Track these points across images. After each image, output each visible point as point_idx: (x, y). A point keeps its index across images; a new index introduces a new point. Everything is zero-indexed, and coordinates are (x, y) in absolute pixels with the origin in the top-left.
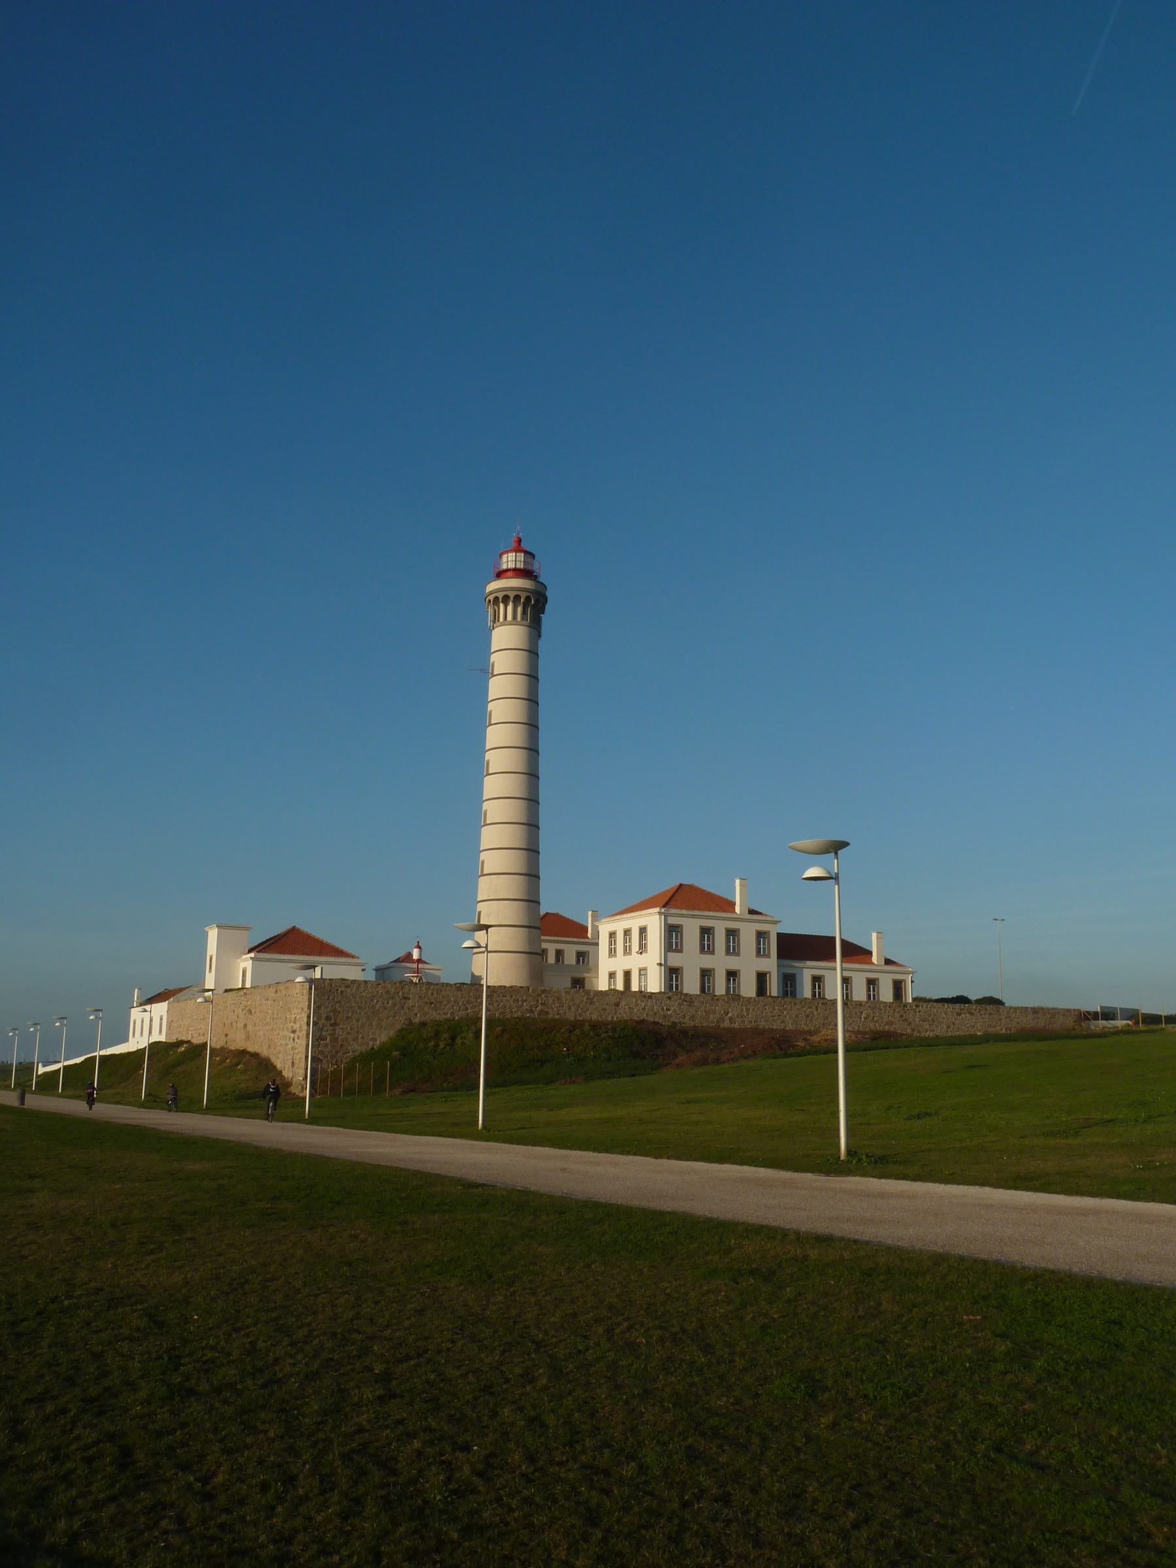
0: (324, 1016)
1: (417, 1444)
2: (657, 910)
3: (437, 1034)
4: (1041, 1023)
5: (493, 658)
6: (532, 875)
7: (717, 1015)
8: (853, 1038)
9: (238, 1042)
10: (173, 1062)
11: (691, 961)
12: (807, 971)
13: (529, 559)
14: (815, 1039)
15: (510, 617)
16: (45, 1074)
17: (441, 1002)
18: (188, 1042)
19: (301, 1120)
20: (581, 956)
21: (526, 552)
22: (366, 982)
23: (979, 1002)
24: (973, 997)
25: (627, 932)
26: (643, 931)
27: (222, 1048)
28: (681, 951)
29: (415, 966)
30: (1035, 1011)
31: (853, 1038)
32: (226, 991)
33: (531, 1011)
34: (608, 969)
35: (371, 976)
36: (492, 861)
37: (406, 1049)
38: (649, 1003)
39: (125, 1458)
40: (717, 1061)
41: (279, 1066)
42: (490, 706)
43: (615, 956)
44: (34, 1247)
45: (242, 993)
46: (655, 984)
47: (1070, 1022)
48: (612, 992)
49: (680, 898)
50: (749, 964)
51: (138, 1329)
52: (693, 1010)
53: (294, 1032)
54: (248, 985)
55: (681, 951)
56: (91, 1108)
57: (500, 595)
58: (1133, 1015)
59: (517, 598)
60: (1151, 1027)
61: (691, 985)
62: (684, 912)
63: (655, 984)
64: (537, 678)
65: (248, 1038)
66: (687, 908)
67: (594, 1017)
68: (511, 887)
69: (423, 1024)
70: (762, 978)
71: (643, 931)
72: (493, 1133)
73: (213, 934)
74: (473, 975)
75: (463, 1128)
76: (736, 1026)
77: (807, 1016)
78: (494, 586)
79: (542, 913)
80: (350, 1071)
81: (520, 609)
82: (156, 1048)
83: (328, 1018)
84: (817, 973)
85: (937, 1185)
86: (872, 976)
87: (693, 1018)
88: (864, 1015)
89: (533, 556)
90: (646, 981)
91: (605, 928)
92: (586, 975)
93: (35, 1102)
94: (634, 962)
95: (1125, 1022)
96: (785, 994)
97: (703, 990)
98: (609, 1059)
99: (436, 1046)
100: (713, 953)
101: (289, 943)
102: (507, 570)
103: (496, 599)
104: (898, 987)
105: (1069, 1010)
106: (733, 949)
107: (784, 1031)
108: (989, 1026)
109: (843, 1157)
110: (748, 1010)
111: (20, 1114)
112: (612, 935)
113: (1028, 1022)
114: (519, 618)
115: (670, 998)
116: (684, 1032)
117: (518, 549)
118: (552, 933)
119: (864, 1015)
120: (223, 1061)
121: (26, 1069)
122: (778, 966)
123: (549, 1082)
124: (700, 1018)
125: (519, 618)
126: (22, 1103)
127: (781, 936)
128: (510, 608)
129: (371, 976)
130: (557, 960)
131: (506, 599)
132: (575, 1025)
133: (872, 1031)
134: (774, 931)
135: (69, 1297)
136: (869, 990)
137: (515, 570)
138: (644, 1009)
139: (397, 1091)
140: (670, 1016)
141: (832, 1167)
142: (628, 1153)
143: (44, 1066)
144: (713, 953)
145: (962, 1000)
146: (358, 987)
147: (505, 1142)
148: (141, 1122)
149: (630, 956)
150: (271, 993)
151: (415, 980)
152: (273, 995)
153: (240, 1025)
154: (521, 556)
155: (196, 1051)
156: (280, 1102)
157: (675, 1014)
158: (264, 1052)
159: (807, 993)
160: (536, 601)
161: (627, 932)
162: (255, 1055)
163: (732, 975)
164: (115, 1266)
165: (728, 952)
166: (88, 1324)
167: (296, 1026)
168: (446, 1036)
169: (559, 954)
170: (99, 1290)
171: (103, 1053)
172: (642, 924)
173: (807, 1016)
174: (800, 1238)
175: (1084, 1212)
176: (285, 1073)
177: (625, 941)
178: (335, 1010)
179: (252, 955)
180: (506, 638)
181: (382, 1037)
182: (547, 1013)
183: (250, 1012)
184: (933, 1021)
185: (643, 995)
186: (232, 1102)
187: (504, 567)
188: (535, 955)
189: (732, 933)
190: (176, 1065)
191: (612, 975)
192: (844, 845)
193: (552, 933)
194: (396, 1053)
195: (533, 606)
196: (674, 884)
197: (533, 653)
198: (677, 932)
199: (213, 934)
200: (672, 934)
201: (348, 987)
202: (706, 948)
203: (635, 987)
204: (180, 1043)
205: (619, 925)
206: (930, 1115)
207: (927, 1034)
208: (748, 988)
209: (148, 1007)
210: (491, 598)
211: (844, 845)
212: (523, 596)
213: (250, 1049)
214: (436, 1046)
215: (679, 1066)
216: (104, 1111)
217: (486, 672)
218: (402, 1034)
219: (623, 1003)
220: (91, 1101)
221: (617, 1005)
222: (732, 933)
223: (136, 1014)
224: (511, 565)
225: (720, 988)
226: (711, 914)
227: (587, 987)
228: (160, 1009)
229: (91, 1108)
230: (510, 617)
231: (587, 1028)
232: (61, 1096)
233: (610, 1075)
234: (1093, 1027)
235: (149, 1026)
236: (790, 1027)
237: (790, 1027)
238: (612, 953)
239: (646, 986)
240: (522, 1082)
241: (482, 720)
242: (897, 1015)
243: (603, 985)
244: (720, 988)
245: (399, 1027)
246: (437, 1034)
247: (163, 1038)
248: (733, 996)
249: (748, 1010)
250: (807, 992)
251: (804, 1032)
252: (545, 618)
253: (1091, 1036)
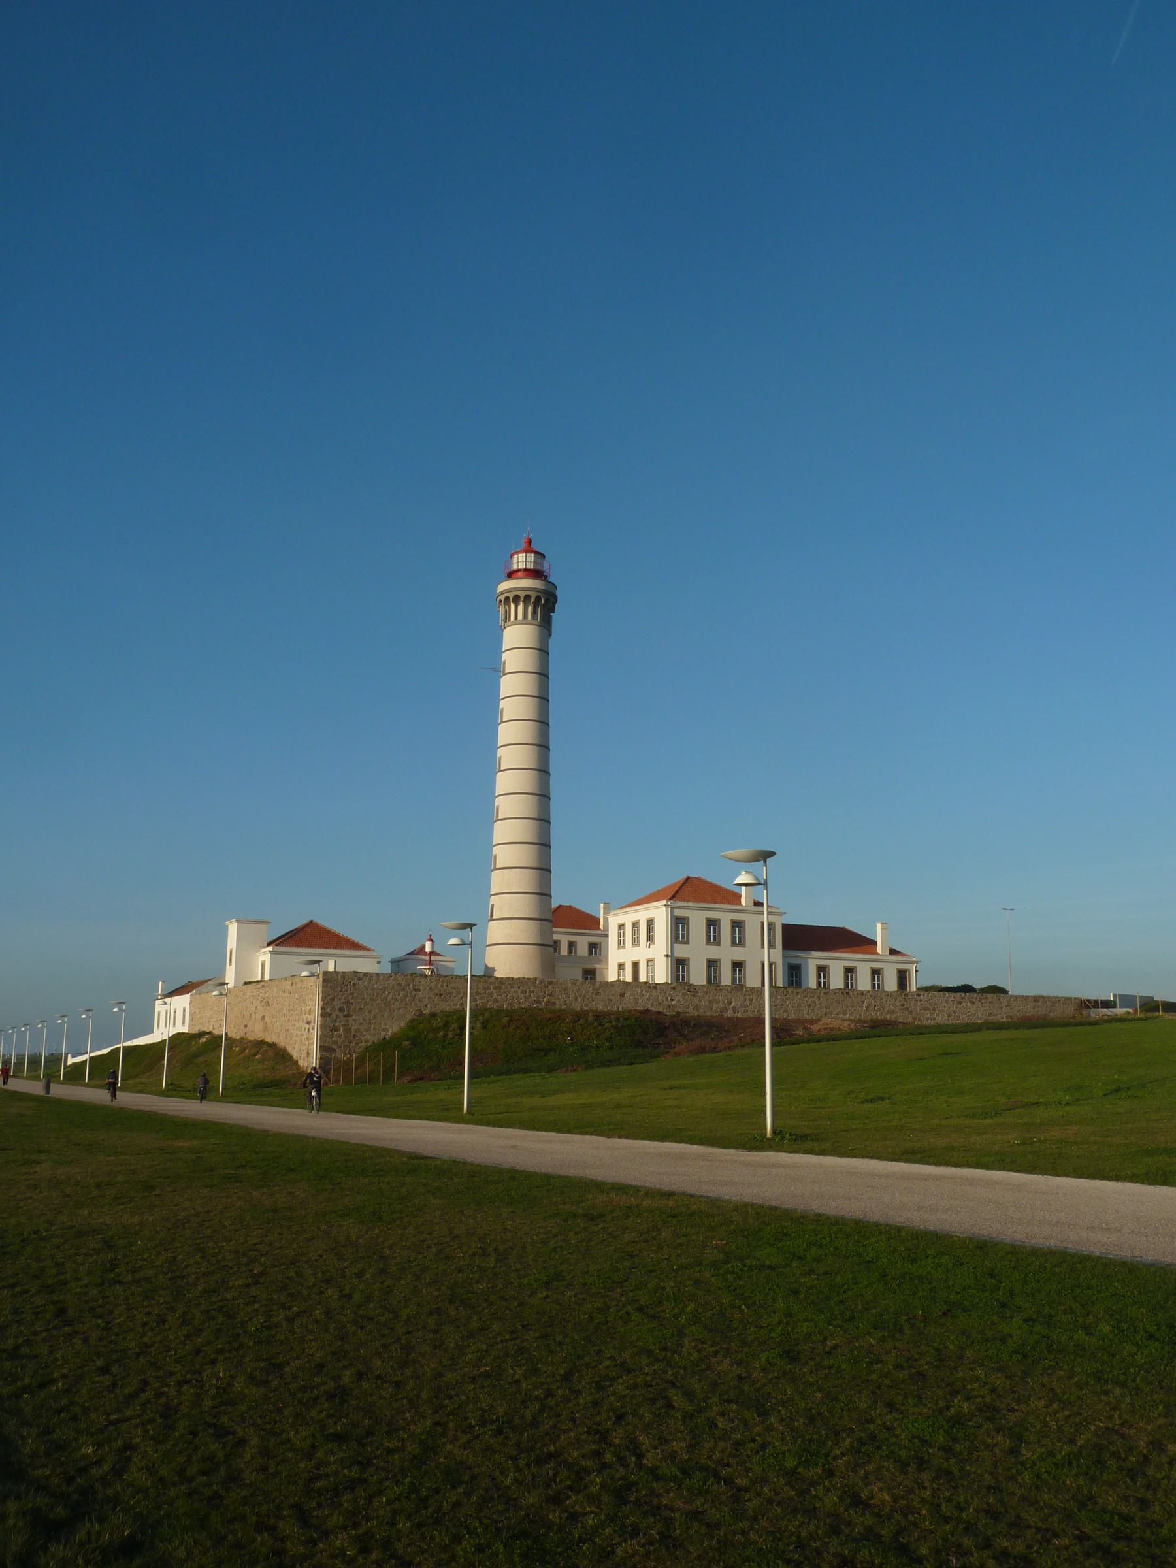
0: (337, 1007)
1: (256, 1306)
2: (664, 902)
3: (447, 1025)
4: (1042, 1010)
5: (505, 656)
6: (543, 869)
7: (721, 1005)
8: (852, 1026)
9: (256, 1033)
10: (194, 1051)
11: (697, 952)
12: (812, 961)
13: (539, 559)
14: (815, 1027)
15: (520, 617)
16: (74, 1064)
17: (450, 994)
18: (210, 1033)
20: (593, 947)
21: (536, 553)
22: (377, 974)
23: (983, 990)
24: (977, 986)
25: (635, 924)
26: (650, 922)
27: (242, 1039)
28: (687, 942)
29: (427, 958)
30: (1036, 999)
31: (852, 1026)
32: (246, 983)
33: (539, 1002)
34: (618, 962)
35: (387, 969)
36: (504, 855)
37: (414, 1039)
38: (654, 993)
39: (62, 1311)
40: (714, 1050)
41: (295, 1055)
42: (502, 704)
43: (638, 945)
44: (30, 1201)
45: (260, 985)
46: (662, 975)
47: (1070, 1011)
48: (620, 982)
49: (689, 890)
51: (94, 1249)
52: (696, 1000)
53: (309, 1023)
54: (267, 978)
55: (687, 942)
57: (511, 595)
58: (1126, 1000)
59: (527, 597)
60: (1150, 1014)
61: (697, 976)
62: (690, 904)
63: (662, 975)
64: (547, 676)
65: (266, 1029)
66: (694, 900)
67: (600, 1007)
68: (522, 880)
69: (434, 1015)
71: (650, 922)
72: (478, 1116)
73: (233, 928)
74: (486, 966)
75: (448, 1112)
76: (739, 1015)
77: (809, 1006)
79: (554, 905)
80: (361, 1060)
81: (530, 609)
82: (178, 1041)
83: (341, 1010)
84: (822, 963)
85: (861, 1160)
86: (876, 965)
87: (696, 1008)
88: (865, 1004)
89: (543, 556)
90: (653, 972)
91: (613, 921)
92: (597, 966)
93: (59, 1091)
94: (641, 953)
95: (1124, 1010)
96: (791, 984)
97: (709, 980)
98: (611, 1048)
99: (445, 1036)
100: (719, 944)
101: (306, 936)
102: (518, 571)
103: (507, 599)
104: (902, 976)
105: (1070, 999)
106: (738, 941)
107: (786, 1020)
108: (990, 1014)
109: (769, 1136)
110: (751, 1000)
111: (44, 1102)
112: (621, 927)
113: (1029, 1010)
114: (529, 617)
115: (674, 988)
116: (686, 1022)
117: (528, 550)
118: (564, 925)
119: (865, 1004)
120: (242, 1051)
121: (54, 1060)
123: (551, 1070)
124: (704, 1008)
125: (529, 617)
126: (48, 1092)
127: (786, 927)
128: (520, 607)
129: (387, 969)
130: (570, 951)
131: (516, 599)
132: (579, 1016)
133: (871, 1020)
134: (779, 922)
135: (47, 1231)
136: (873, 979)
137: (525, 570)
138: (648, 999)
139: (406, 1080)
140: (675, 1006)
141: (757, 1143)
142: (586, 1133)
143: (73, 1057)
144: (719, 944)
145: (967, 989)
146: (370, 980)
147: (482, 1125)
148: (155, 1109)
149: (638, 949)
150: (287, 985)
151: (427, 972)
152: (289, 987)
153: (259, 1016)
154: (531, 557)
155: (215, 1041)
156: (324, 1089)
157: (680, 1004)
158: (281, 1042)
159: (813, 984)
161: (635, 924)
162: (273, 1046)
163: (738, 965)
164: (90, 1214)
165: (734, 943)
166: (58, 1247)
167: (311, 1018)
168: (454, 1026)
169: (572, 945)
170: (72, 1227)
171: (126, 1044)
172: (650, 916)
173: (809, 1006)
174: (649, 1193)
175: (926, 1178)
176: (301, 1063)
177: (634, 933)
178: (347, 1002)
179: (270, 948)
180: (517, 637)
181: (393, 1027)
182: (554, 1004)
183: (268, 1003)
184: (934, 1009)
186: (240, 1092)
187: (515, 567)
188: (547, 948)
189: (737, 925)
190: (197, 1056)
191: (621, 966)
192: (772, 854)
193: (564, 925)
194: (406, 1043)
195: (544, 606)
196: (681, 877)
197: (543, 651)
198: (683, 925)
199: (233, 928)
200: (679, 926)
201: (360, 979)
202: (712, 938)
203: (643, 979)
204: (202, 1034)
205: (627, 917)
206: (882, 1099)
207: (927, 1023)
209: (167, 1000)
210: (502, 597)
211: (772, 854)
212: (533, 595)
213: (268, 1040)
214: (445, 1036)
215: (677, 1054)
216: (126, 1099)
217: (497, 670)
218: (413, 1024)
219: (628, 994)
220: (112, 1088)
221: (622, 995)
222: (737, 925)
223: (159, 1007)
224: (522, 566)
225: (726, 978)
226: (717, 906)
227: (598, 978)
228: (182, 1002)
230: (520, 617)
231: (590, 1019)
232: (86, 1085)
233: (610, 1063)
234: (1093, 1015)
235: (172, 1018)
236: (792, 1016)
237: (793, 1016)
238: (621, 944)
239: (653, 977)
240: (527, 1070)
241: (494, 718)
242: (898, 1004)
243: (612, 976)
244: (726, 978)
245: (409, 1017)
246: (447, 1025)
247: (186, 1030)
248: (738, 986)
249: (751, 1000)
250: (812, 982)
251: (807, 1021)
252: (555, 617)
253: (1095, 1023)
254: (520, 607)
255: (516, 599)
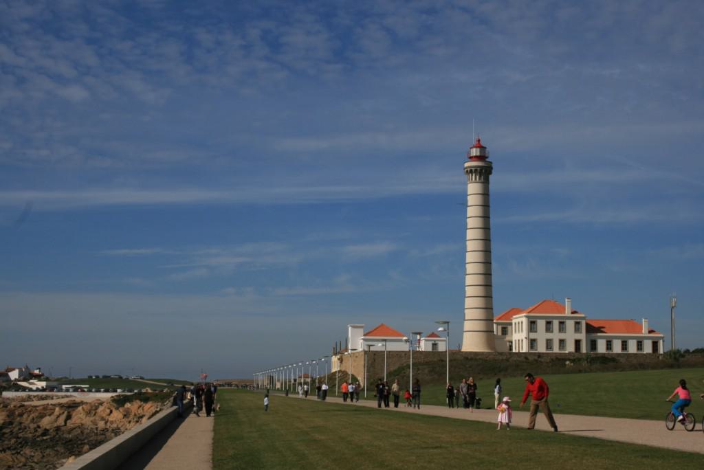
11: (541, 336)
15: (474, 179)
19: (335, 396)
23: (694, 352)
25: (519, 323)
26: (522, 323)
28: (536, 332)
50: (570, 336)
56: (306, 397)
59: (476, 170)
70: (578, 343)
73: (350, 328)
78: (467, 165)
81: (478, 177)
89: (485, 148)
104: (655, 345)
122: (587, 337)
128: (474, 175)
137: (476, 157)
144: (552, 332)
149: (519, 339)
154: (478, 150)
160: (486, 171)
185: (519, 354)
187: (472, 155)
195: (484, 173)
203: (514, 351)
208: (570, 348)
212: (479, 169)
224: (475, 155)
229: (306, 397)
230: (474, 179)
254: (474, 175)
255: (471, 171)
